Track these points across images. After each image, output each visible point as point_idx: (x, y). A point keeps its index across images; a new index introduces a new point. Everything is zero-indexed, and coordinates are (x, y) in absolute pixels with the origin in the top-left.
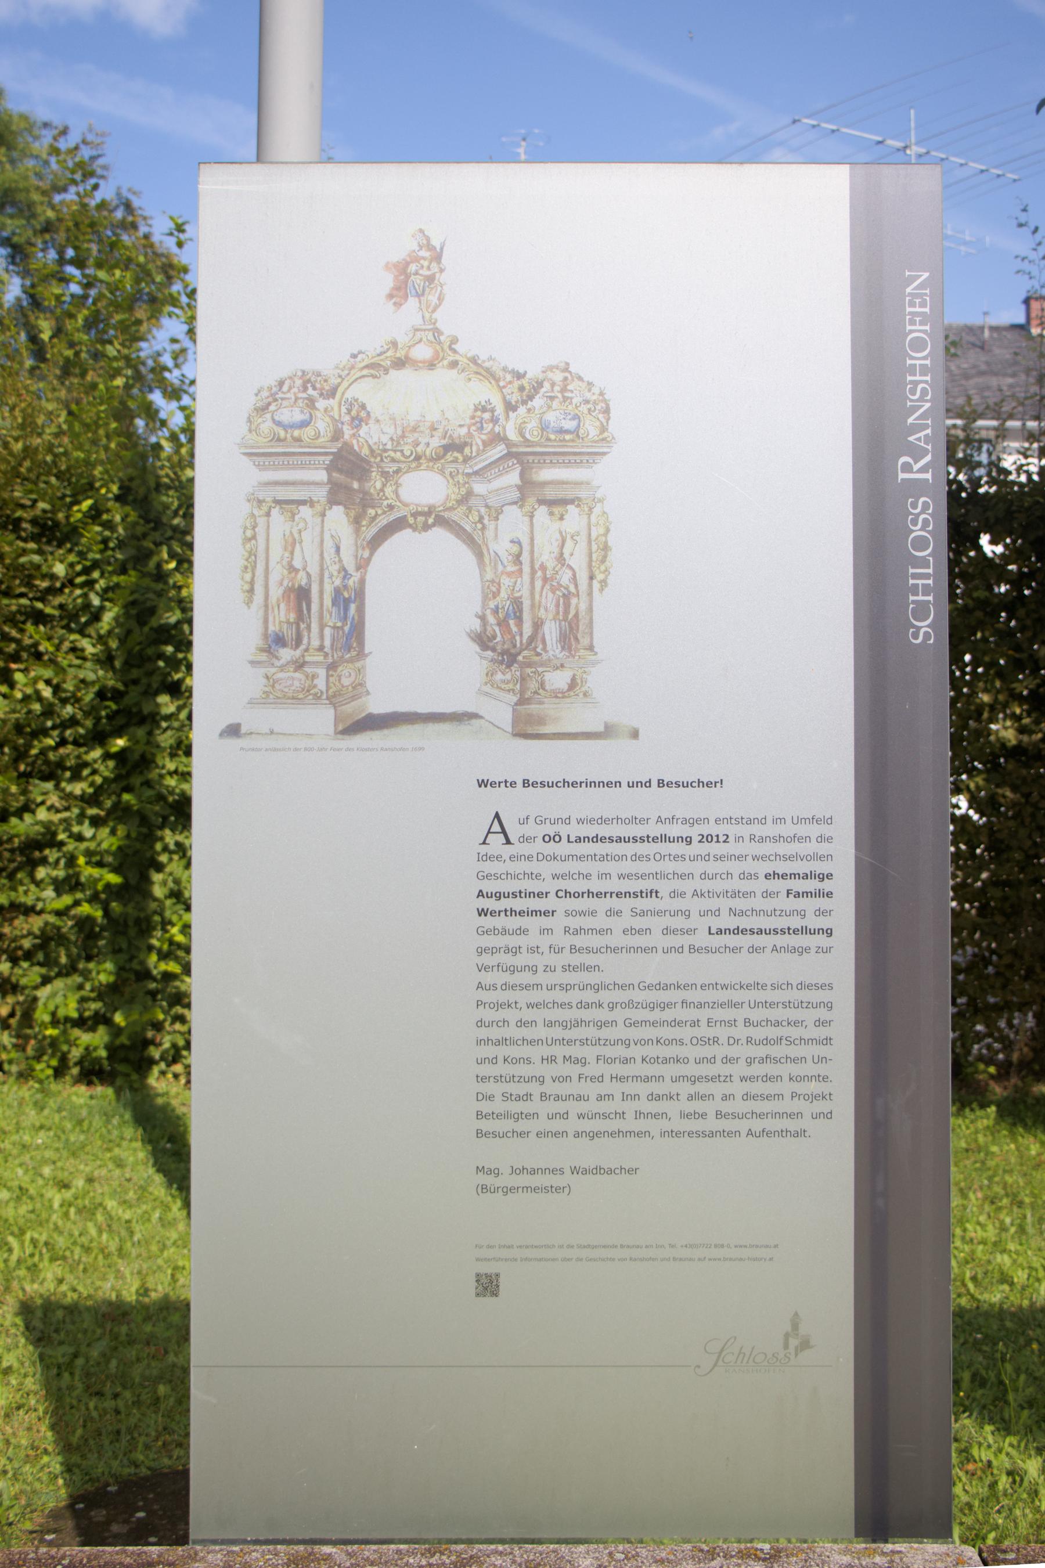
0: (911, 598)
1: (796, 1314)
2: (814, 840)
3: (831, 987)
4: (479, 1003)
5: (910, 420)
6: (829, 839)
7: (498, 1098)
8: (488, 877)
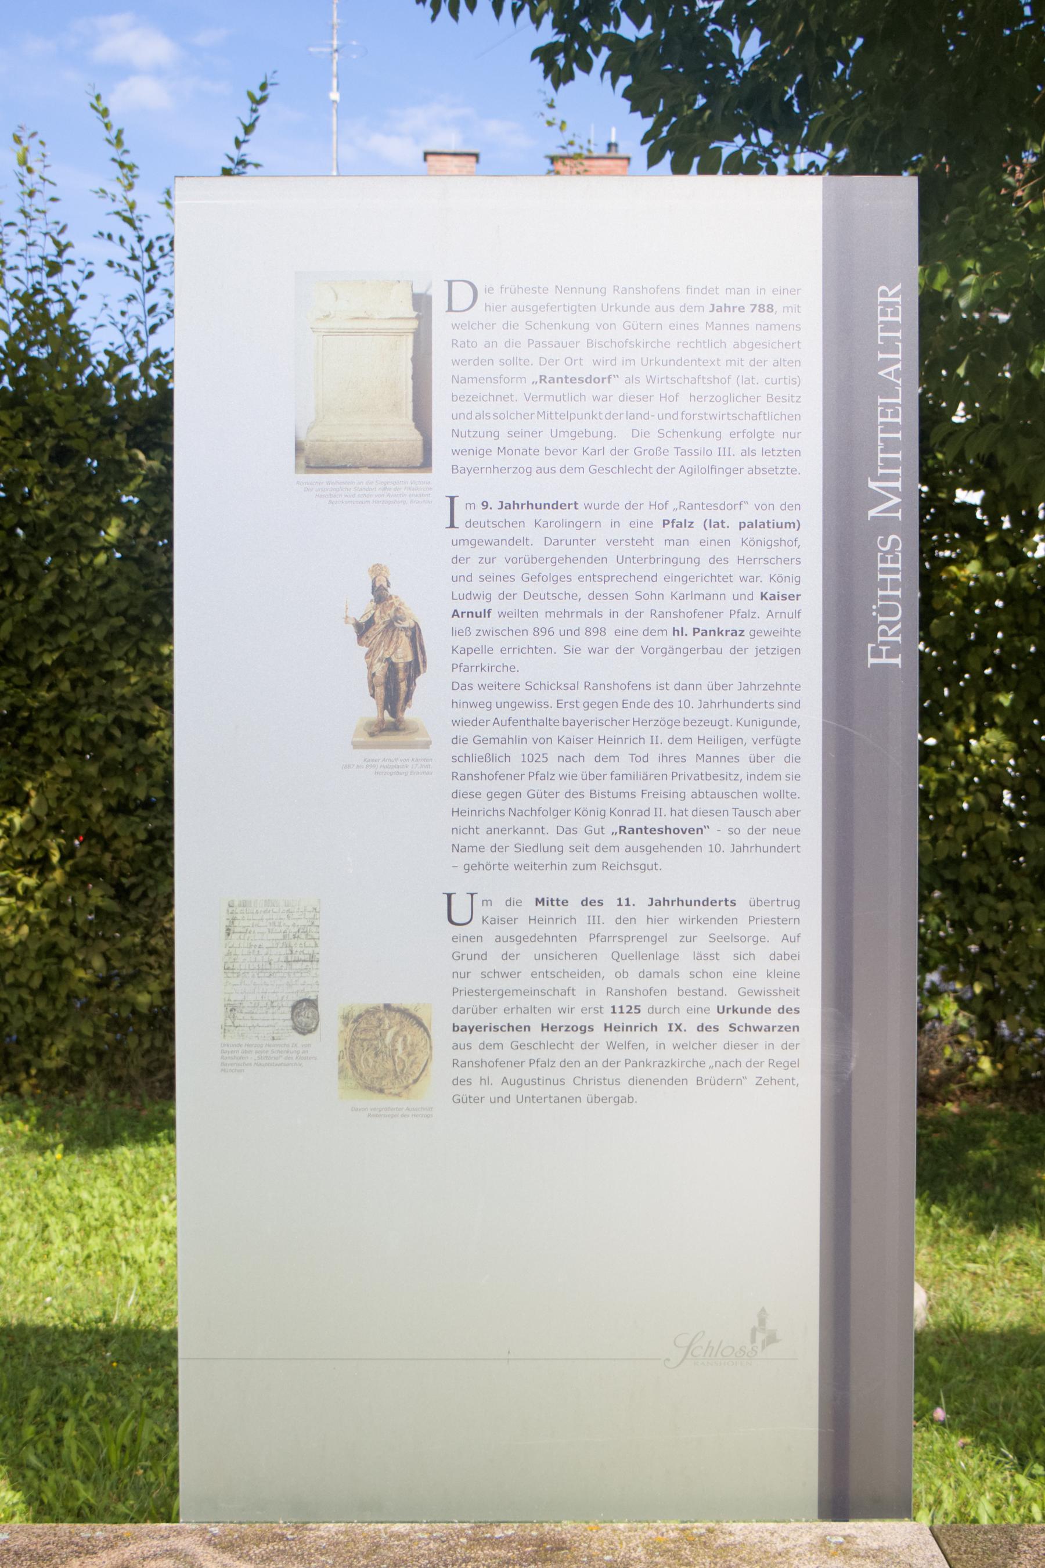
1: (763, 1310)
3: (797, 687)
6: (797, 759)
8: (464, 1011)
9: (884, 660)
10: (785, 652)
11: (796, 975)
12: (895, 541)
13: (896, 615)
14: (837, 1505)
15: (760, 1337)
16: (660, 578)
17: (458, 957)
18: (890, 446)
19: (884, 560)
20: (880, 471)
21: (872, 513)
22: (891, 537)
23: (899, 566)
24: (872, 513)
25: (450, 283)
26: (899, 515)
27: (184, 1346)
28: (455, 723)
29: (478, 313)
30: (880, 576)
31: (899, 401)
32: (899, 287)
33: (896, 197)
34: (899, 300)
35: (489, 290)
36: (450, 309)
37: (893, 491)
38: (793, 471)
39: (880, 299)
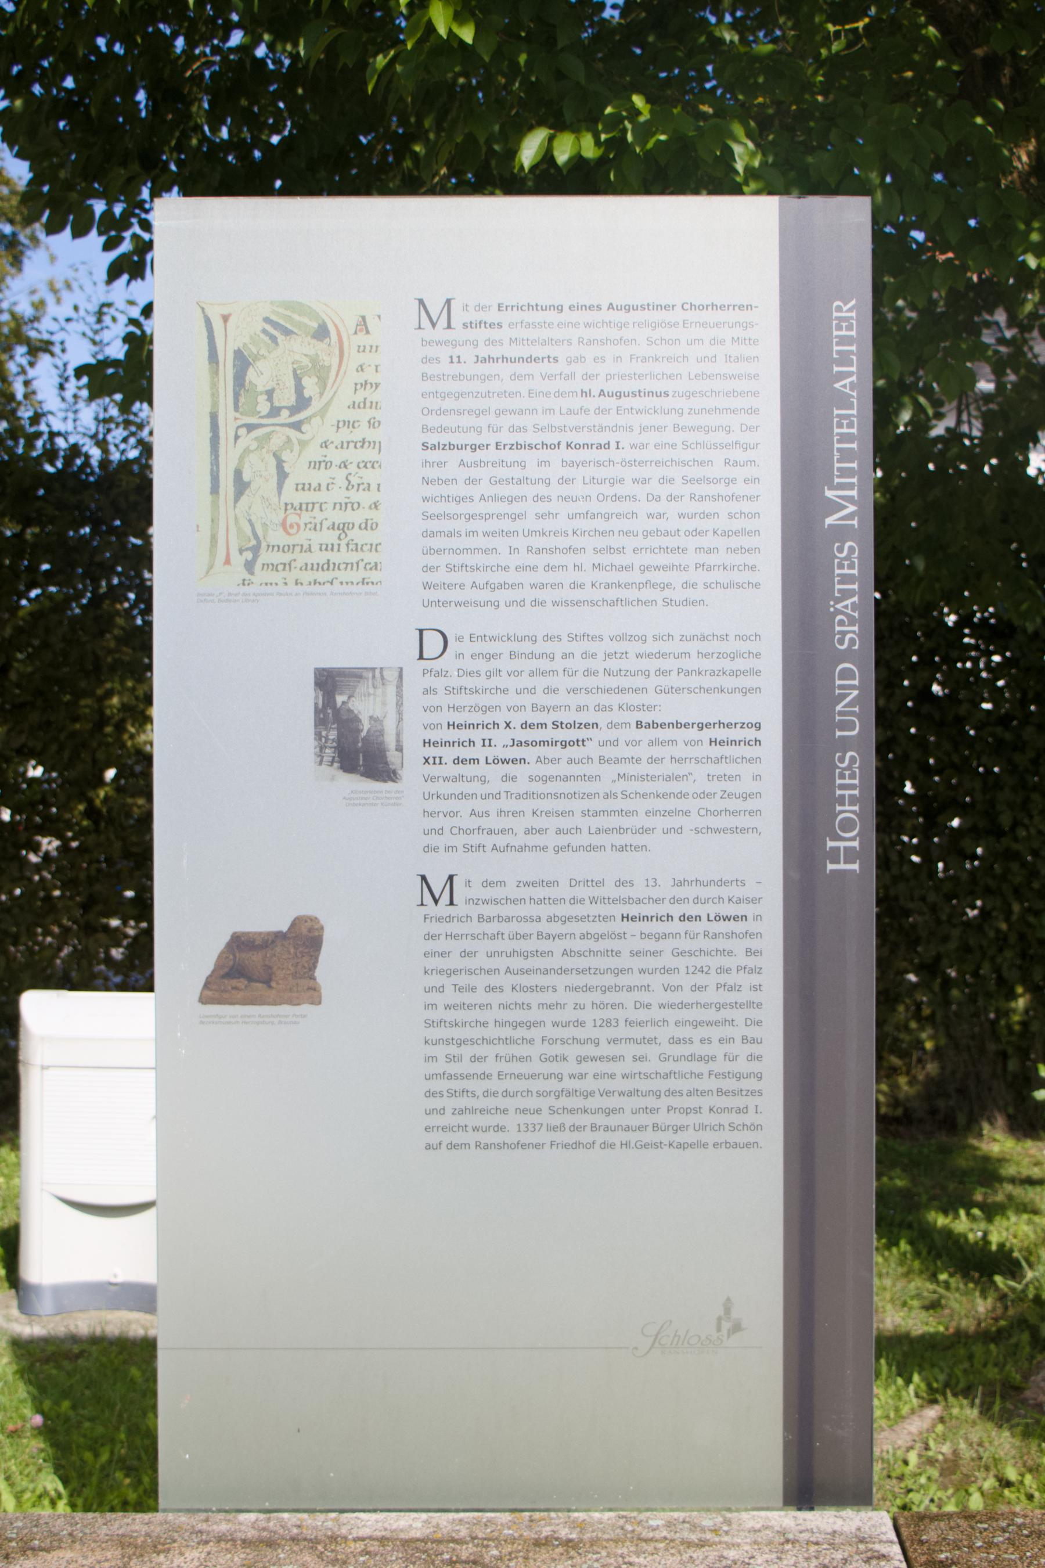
1: (728, 1299)
4: (425, 463)
6: (759, 1058)
9: (842, 866)
10: (745, 691)
11: (755, 394)
12: (852, 758)
13: (854, 729)
14: (804, 1491)
16: (622, 743)
17: (429, 551)
18: (846, 455)
19: (842, 776)
20: (837, 480)
21: (829, 521)
22: (849, 754)
23: (856, 782)
24: (829, 521)
25: (421, 631)
26: (855, 522)
27: (167, 1367)
29: (448, 662)
30: (838, 792)
31: (854, 412)
32: (853, 302)
33: (847, 222)
34: (854, 314)
35: (459, 639)
36: (421, 657)
37: (850, 499)
38: (757, 586)
39: (838, 629)
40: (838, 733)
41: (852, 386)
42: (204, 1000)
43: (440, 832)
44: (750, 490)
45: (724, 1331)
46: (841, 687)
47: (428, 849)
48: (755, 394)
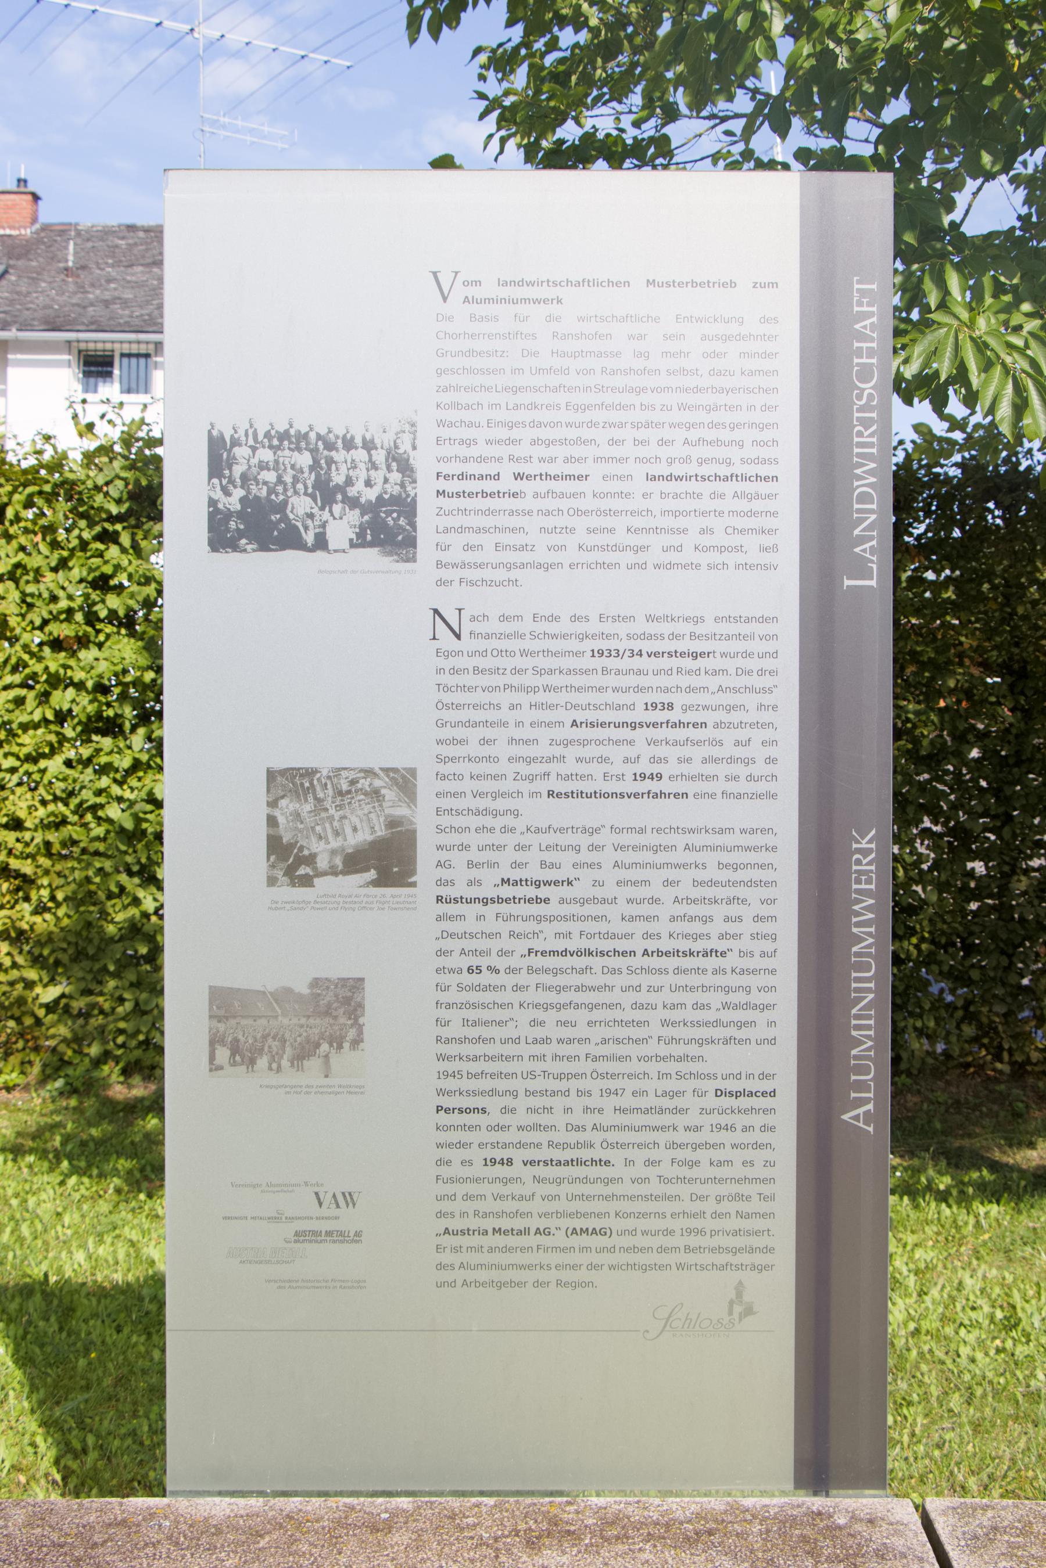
0: (856, 361)
1: (740, 1282)
2: (757, 1129)
5: (856, 532)
6: (772, 1129)
7: (454, 988)
13: (869, 971)
15: (738, 1309)
28: (439, 1146)
32: (873, 832)
34: (873, 868)
37: (868, 1037)
38: (774, 796)
39: (854, 868)
40: (853, 1078)
41: (868, 1117)
42: (210, 987)
43: (453, 1197)
44: (764, 1207)
45: (736, 1316)
46: (859, 511)
47: (441, 583)
48: (773, 972)
